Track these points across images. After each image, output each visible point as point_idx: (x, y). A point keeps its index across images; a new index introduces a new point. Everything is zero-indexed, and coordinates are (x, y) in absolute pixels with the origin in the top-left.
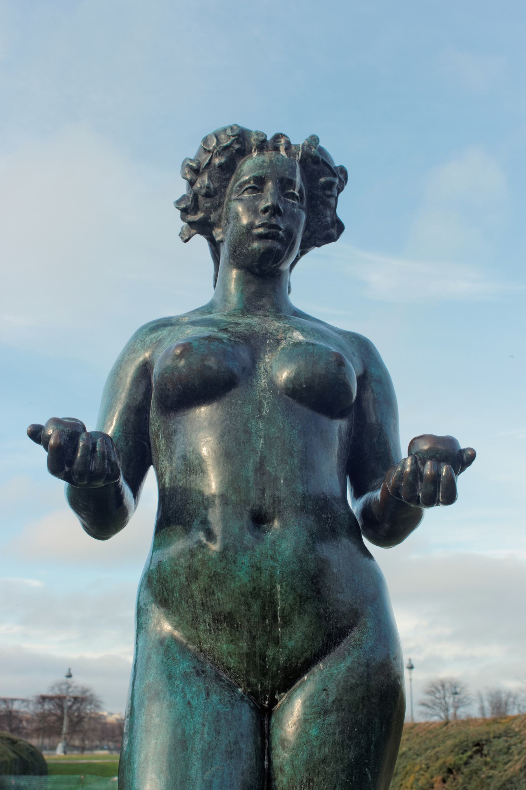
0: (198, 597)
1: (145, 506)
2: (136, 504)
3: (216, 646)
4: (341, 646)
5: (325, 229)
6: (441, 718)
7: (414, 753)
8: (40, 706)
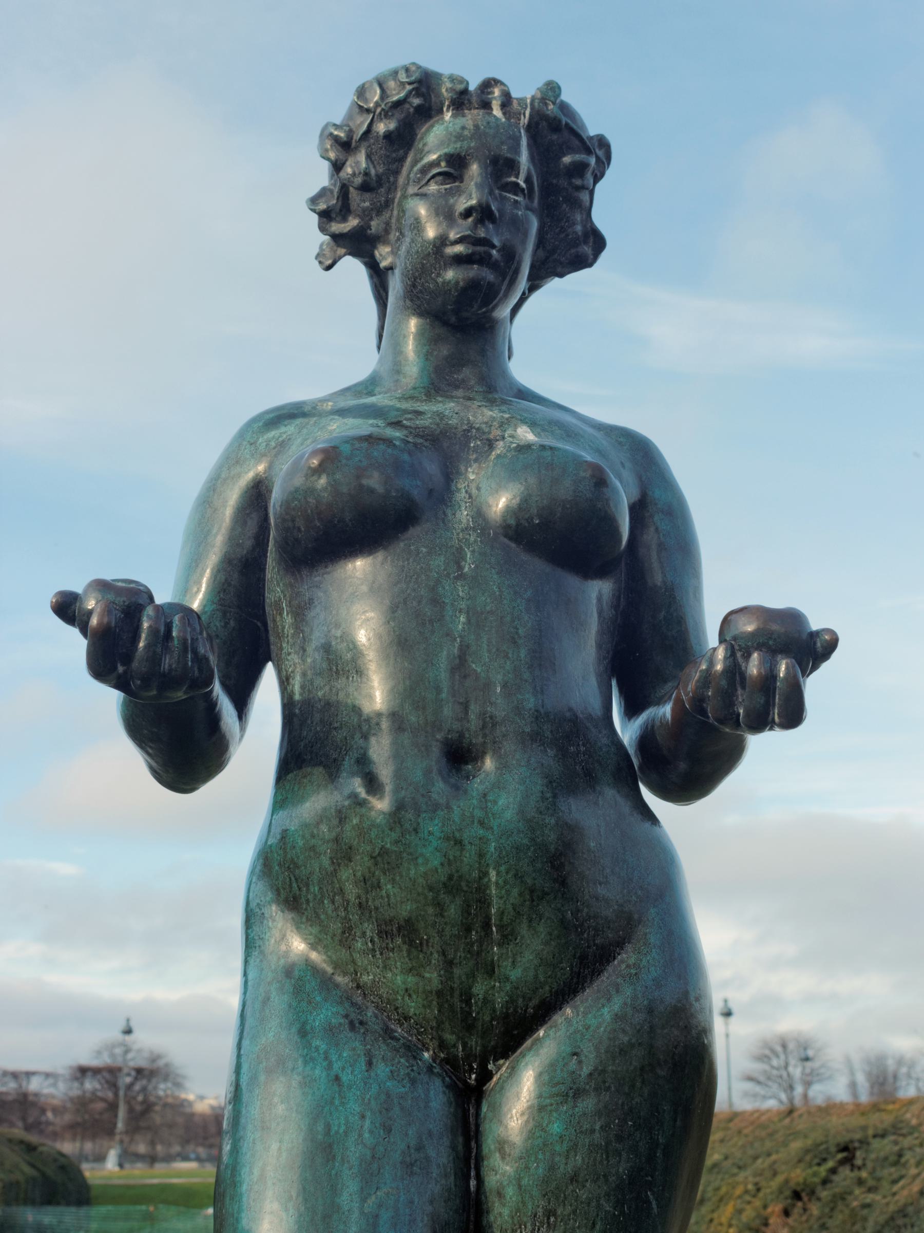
0: (352, 892)
1: (258, 734)
2: (243, 729)
3: (384, 977)
4: (604, 977)
5: (572, 246)
6: (781, 1102)
7: (734, 1164)
8: (76, 1084)
